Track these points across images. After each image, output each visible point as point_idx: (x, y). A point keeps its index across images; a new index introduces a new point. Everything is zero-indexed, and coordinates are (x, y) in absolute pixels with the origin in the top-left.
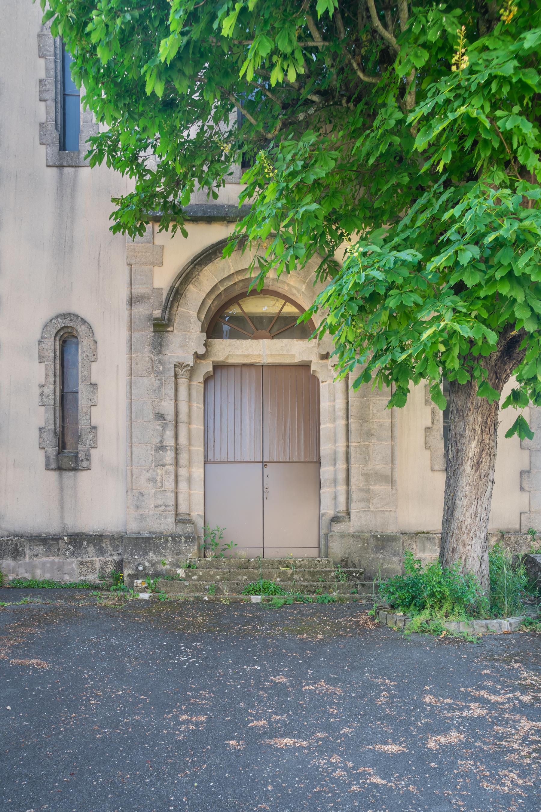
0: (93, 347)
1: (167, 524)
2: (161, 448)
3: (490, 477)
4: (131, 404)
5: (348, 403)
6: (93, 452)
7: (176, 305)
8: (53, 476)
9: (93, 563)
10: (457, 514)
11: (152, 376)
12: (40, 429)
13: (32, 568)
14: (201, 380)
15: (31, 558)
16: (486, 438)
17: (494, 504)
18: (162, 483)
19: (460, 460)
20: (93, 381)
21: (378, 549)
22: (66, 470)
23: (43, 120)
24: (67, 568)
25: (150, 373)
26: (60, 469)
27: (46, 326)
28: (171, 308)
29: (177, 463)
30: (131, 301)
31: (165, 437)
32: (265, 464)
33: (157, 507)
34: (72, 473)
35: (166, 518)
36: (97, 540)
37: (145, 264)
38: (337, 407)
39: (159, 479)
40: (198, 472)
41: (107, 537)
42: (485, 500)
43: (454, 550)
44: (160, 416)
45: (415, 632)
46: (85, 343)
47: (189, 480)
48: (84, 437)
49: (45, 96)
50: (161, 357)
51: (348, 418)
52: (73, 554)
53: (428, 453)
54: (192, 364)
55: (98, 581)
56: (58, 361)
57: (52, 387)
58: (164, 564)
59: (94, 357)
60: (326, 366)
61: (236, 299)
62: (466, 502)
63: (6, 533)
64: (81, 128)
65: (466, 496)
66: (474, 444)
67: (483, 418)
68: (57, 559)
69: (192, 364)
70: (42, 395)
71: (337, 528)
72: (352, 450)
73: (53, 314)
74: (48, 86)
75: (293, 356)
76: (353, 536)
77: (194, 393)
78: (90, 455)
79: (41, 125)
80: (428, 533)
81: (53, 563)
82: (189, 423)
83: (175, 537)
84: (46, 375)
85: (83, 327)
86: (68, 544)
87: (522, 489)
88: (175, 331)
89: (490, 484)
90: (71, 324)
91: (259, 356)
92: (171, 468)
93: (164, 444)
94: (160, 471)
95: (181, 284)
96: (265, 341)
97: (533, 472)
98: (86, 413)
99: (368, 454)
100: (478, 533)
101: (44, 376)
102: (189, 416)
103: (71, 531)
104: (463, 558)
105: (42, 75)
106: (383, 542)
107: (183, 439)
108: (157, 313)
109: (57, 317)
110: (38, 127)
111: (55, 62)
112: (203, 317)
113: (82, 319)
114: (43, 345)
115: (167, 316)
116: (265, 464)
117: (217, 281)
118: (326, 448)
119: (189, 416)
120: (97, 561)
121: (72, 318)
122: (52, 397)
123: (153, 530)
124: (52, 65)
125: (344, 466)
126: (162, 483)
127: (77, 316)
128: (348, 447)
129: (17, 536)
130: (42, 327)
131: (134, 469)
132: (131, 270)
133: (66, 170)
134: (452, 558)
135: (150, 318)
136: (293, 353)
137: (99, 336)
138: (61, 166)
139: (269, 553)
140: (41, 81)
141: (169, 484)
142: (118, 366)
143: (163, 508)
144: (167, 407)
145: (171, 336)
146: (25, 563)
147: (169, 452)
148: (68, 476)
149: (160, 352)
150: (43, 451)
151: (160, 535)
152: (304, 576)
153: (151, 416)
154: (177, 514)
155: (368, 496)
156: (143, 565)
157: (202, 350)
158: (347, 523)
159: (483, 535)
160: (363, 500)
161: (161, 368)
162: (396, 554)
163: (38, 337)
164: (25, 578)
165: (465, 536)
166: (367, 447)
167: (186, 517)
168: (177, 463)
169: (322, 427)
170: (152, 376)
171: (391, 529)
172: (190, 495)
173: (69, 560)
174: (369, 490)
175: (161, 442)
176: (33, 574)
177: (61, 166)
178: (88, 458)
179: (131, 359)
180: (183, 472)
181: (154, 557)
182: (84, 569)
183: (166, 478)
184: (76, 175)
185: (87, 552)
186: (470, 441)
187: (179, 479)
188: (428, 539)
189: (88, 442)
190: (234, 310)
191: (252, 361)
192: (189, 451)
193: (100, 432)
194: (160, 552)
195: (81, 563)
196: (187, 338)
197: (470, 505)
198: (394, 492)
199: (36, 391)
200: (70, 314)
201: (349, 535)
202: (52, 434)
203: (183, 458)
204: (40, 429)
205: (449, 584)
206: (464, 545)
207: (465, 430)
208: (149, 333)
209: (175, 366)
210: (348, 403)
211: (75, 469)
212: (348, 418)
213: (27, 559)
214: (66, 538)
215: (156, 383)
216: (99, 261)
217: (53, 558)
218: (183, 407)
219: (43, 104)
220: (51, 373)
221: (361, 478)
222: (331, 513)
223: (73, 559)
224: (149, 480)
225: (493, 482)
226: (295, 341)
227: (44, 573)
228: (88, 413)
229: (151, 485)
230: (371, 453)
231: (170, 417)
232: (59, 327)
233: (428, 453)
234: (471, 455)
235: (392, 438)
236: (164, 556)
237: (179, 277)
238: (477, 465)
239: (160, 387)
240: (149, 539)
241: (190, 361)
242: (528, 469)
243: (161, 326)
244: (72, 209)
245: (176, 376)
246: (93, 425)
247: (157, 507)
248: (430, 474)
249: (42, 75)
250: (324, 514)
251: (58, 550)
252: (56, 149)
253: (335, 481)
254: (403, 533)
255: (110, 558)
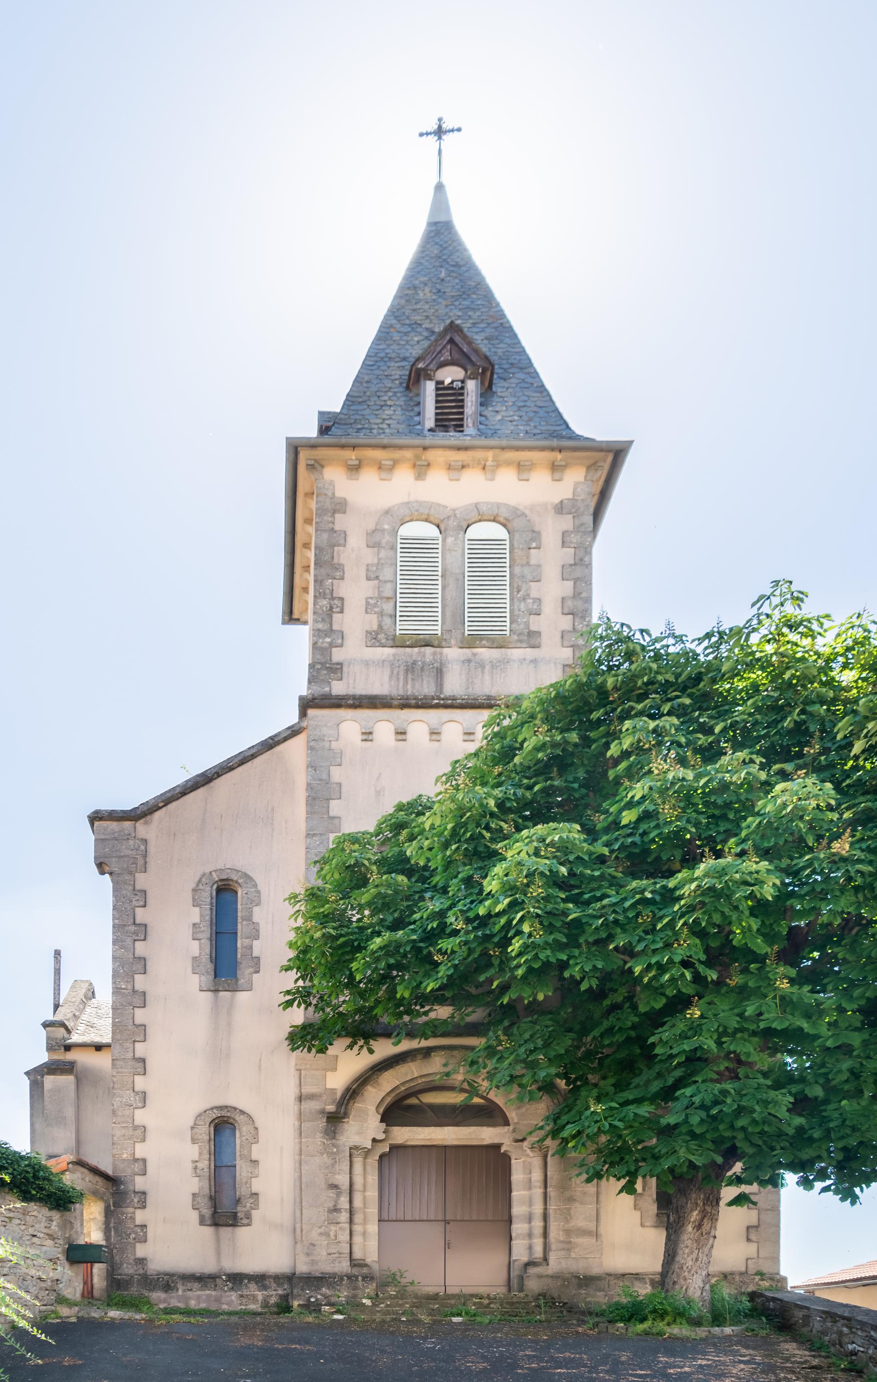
0: (253, 1132)
1: (343, 1266)
2: (336, 1210)
3: (712, 1234)
4: (300, 1177)
5: (546, 1176)
6: (254, 1212)
7: (352, 1102)
8: (208, 1231)
9: (254, 1297)
10: (678, 1258)
11: (325, 1156)
12: (194, 1195)
13: (187, 1299)
14: (377, 1158)
15: (184, 1291)
16: (708, 1209)
17: (715, 1252)
18: (336, 1236)
19: (681, 1224)
20: (254, 1158)
21: (580, 1286)
22: (223, 1225)
23: (197, 954)
24: (224, 1300)
25: (322, 1154)
26: (216, 1224)
27: (200, 1115)
28: (347, 1105)
29: (351, 1221)
30: (300, 1099)
31: (340, 1202)
32: (447, 1222)
33: (330, 1254)
34: (230, 1229)
35: (340, 1262)
36: (260, 1279)
37: (318, 1070)
38: (533, 1179)
39: (332, 1234)
40: (373, 1228)
41: (270, 1277)
42: (706, 1250)
43: (674, 1283)
44: (334, 1187)
45: (638, 1334)
46: (244, 1129)
47: (364, 1234)
48: (243, 1201)
49: (199, 936)
50: (334, 1141)
51: (546, 1187)
52: (232, 1289)
53: (638, 1213)
54: (370, 1147)
55: (260, 1310)
56: (213, 1143)
57: (207, 1162)
58: (339, 1297)
59: (256, 1139)
60: (522, 1147)
61: (416, 1093)
62: (687, 1251)
63: (155, 1273)
64: (239, 960)
65: (687, 1247)
66: (695, 1213)
67: (705, 1195)
68: (214, 1293)
69: (370, 1147)
70: (196, 1168)
71: (532, 1270)
72: (551, 1212)
73: (208, 1106)
74: (203, 929)
75: (483, 1139)
76: (552, 1277)
77: (369, 1168)
78: (250, 1215)
79: (194, 959)
80: (637, 1274)
81: (209, 1296)
82: (365, 1190)
83: (349, 1277)
84: (200, 1154)
85: (242, 1117)
86: (226, 1281)
87: (748, 1240)
88: (351, 1122)
89: (712, 1239)
90: (229, 1114)
91: (444, 1139)
92: (347, 1226)
93: (339, 1207)
94: (333, 1228)
95: (358, 1086)
96: (450, 1128)
97: (762, 1227)
98: (246, 1183)
99: (570, 1214)
100: (699, 1272)
101: (197, 1154)
102: (365, 1186)
103: (228, 1271)
104: (684, 1288)
105: (197, 920)
106: (587, 1281)
107: (358, 1203)
108: (331, 1108)
109: (212, 1109)
110: (190, 961)
111: (211, 909)
112: (381, 1111)
113: (241, 1111)
114: (196, 1130)
115: (342, 1111)
116: (447, 1222)
117: (398, 1083)
118: (517, 1210)
119: (365, 1186)
120: (260, 1295)
121: (229, 1109)
122: (206, 1170)
123: (324, 1271)
124: (208, 912)
125: (542, 1224)
126: (336, 1236)
127: (235, 1109)
128: (545, 1209)
129: (168, 1275)
130: (195, 1116)
131: (304, 1226)
132: (300, 1074)
133: (222, 994)
134: (673, 1288)
135: (322, 1112)
136: (483, 1137)
137: (259, 1123)
138: (216, 991)
139: (450, 1291)
140: (194, 925)
141: (344, 1237)
142: (282, 1148)
143: (337, 1255)
144: (343, 1180)
145: (346, 1126)
146: (178, 1296)
147: (344, 1214)
148: (225, 1232)
149: (334, 1138)
150: (197, 1211)
151: (333, 1276)
152: (501, 1305)
153: (324, 1186)
154: (351, 1260)
155: (568, 1247)
156: (316, 1297)
157: (381, 1136)
158: (545, 1267)
159: (704, 1273)
160: (563, 1249)
161: (335, 1150)
162: (600, 1290)
163: (191, 1123)
164: (178, 1307)
165: (686, 1274)
166: (569, 1209)
167: (361, 1262)
168: (351, 1221)
169: (514, 1194)
170: (325, 1156)
171: (595, 1271)
172: (364, 1245)
173: (227, 1294)
174: (570, 1242)
175: (335, 1206)
176: (187, 1304)
177: (216, 991)
178: (248, 1216)
179: (300, 1143)
180: (357, 1228)
181: (328, 1291)
182: (244, 1300)
183: (340, 1233)
184: (233, 998)
185: (247, 1287)
186: (692, 1211)
187: (354, 1233)
188: (637, 1279)
189: (248, 1205)
190: (413, 1101)
191: (435, 1143)
192: (365, 1213)
193: (261, 1198)
194: (333, 1287)
195: (242, 1296)
196: (365, 1126)
197: (692, 1253)
198: (599, 1243)
199: (190, 1166)
200: (227, 1107)
201: (547, 1276)
202: (206, 1200)
203: (358, 1218)
204: (194, 1195)
205: (670, 1304)
206: (685, 1279)
207: (687, 1203)
208: (322, 1123)
209: (351, 1148)
210: (546, 1176)
211: (234, 1225)
212: (546, 1187)
213: (180, 1292)
214: (224, 1277)
215: (329, 1161)
216: (260, 1066)
217: (208, 1292)
218: (358, 1180)
219: (197, 942)
220: (206, 1152)
221: (561, 1233)
222: (525, 1259)
223: (232, 1293)
224: (321, 1234)
225: (715, 1237)
226: (485, 1128)
227: (199, 1303)
228: (248, 1182)
229: (323, 1238)
230: (572, 1213)
231: (345, 1186)
232: (215, 1116)
233: (638, 1213)
234: (692, 1220)
235: (597, 1202)
236: (339, 1291)
237: (356, 1080)
238: (699, 1226)
239: (333, 1165)
240: (322, 1278)
241: (368, 1144)
242: (756, 1224)
243: (335, 1119)
244: (229, 1024)
245: (351, 1156)
246: (254, 1191)
247: (330, 1254)
248: (641, 1229)
249: (197, 920)
250: (515, 1261)
251: (216, 1286)
252: (212, 977)
253: (530, 1235)
254: (610, 1275)
255: (274, 1293)
